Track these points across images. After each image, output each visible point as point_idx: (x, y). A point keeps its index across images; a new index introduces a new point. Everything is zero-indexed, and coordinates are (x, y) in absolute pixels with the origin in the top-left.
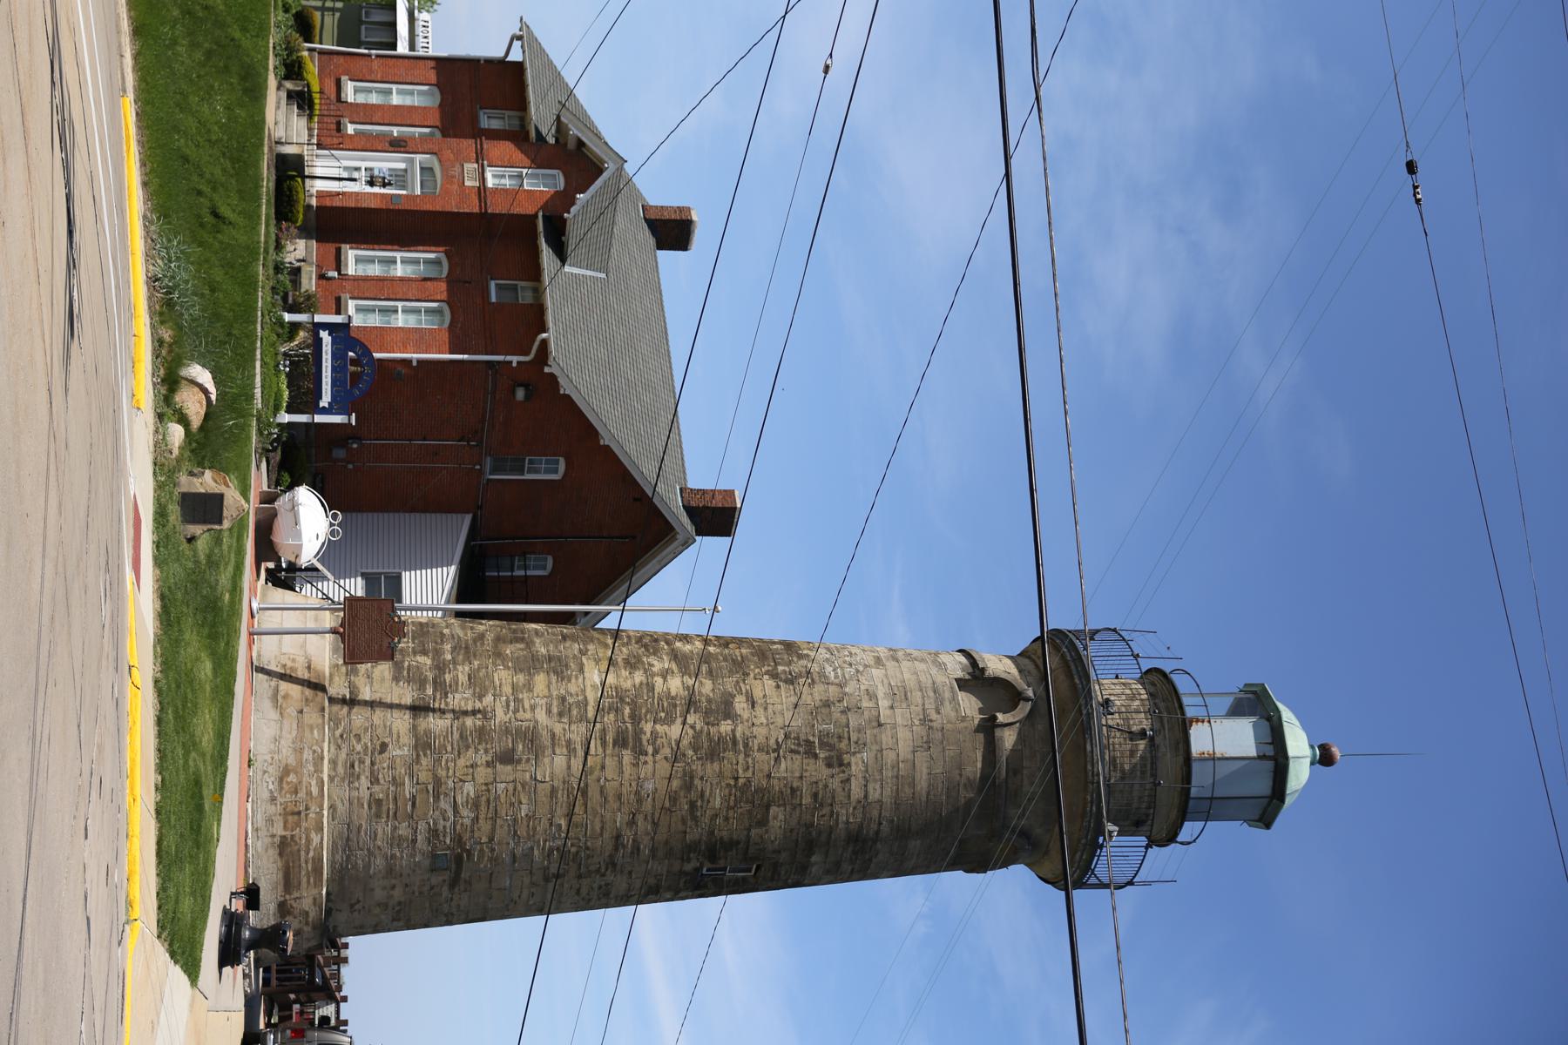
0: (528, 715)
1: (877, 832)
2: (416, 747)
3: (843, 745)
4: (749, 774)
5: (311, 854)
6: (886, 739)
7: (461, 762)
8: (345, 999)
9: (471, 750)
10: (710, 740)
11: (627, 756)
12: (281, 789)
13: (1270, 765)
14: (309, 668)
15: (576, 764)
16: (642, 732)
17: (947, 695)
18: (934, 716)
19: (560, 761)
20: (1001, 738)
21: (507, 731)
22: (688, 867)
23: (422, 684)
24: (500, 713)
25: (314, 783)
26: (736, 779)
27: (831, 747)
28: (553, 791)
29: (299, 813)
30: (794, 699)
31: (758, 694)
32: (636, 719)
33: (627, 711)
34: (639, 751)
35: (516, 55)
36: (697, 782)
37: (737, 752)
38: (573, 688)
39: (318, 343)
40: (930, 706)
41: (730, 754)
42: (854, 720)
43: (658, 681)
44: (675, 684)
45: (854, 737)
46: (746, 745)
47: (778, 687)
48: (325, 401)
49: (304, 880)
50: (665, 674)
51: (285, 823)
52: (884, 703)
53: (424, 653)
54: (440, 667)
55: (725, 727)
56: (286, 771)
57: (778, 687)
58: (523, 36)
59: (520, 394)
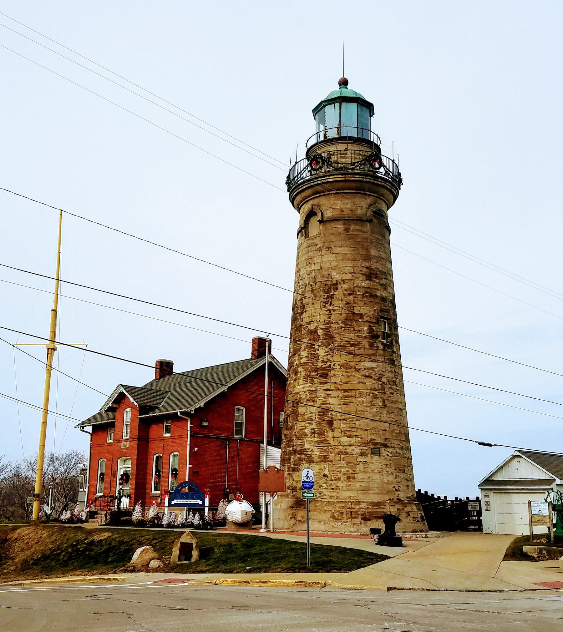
0: (314, 415)
1: (367, 268)
2: (325, 462)
3: (329, 283)
4: (340, 322)
5: (370, 507)
6: (327, 265)
7: (332, 443)
8: (468, 498)
9: (327, 438)
10: (325, 339)
11: (331, 373)
12: (340, 519)
13: (344, 105)
14: (292, 507)
15: (334, 394)
16: (321, 367)
17: (311, 241)
18: (318, 246)
19: (333, 401)
20: (327, 218)
21: (320, 423)
22: (381, 347)
23: (301, 459)
24: (313, 426)
25: (339, 505)
26: (341, 327)
27: (330, 288)
28: (346, 404)
29: (351, 512)
30: (310, 305)
31: (308, 320)
32: (316, 370)
33: (313, 374)
34: (329, 368)
35: (89, 429)
36: (342, 344)
37: (331, 327)
38: (303, 396)
39: (176, 505)
40: (314, 248)
41: (331, 330)
42: (319, 279)
43: (302, 361)
44: (304, 353)
45: (326, 279)
46: (328, 324)
47: (305, 311)
48: (200, 502)
49: (381, 510)
50: (300, 359)
51: (355, 518)
52: (313, 267)
53: (290, 459)
54: (295, 452)
55: (320, 332)
56: (333, 517)
57: (305, 311)
58: (82, 426)
59: (205, 424)
